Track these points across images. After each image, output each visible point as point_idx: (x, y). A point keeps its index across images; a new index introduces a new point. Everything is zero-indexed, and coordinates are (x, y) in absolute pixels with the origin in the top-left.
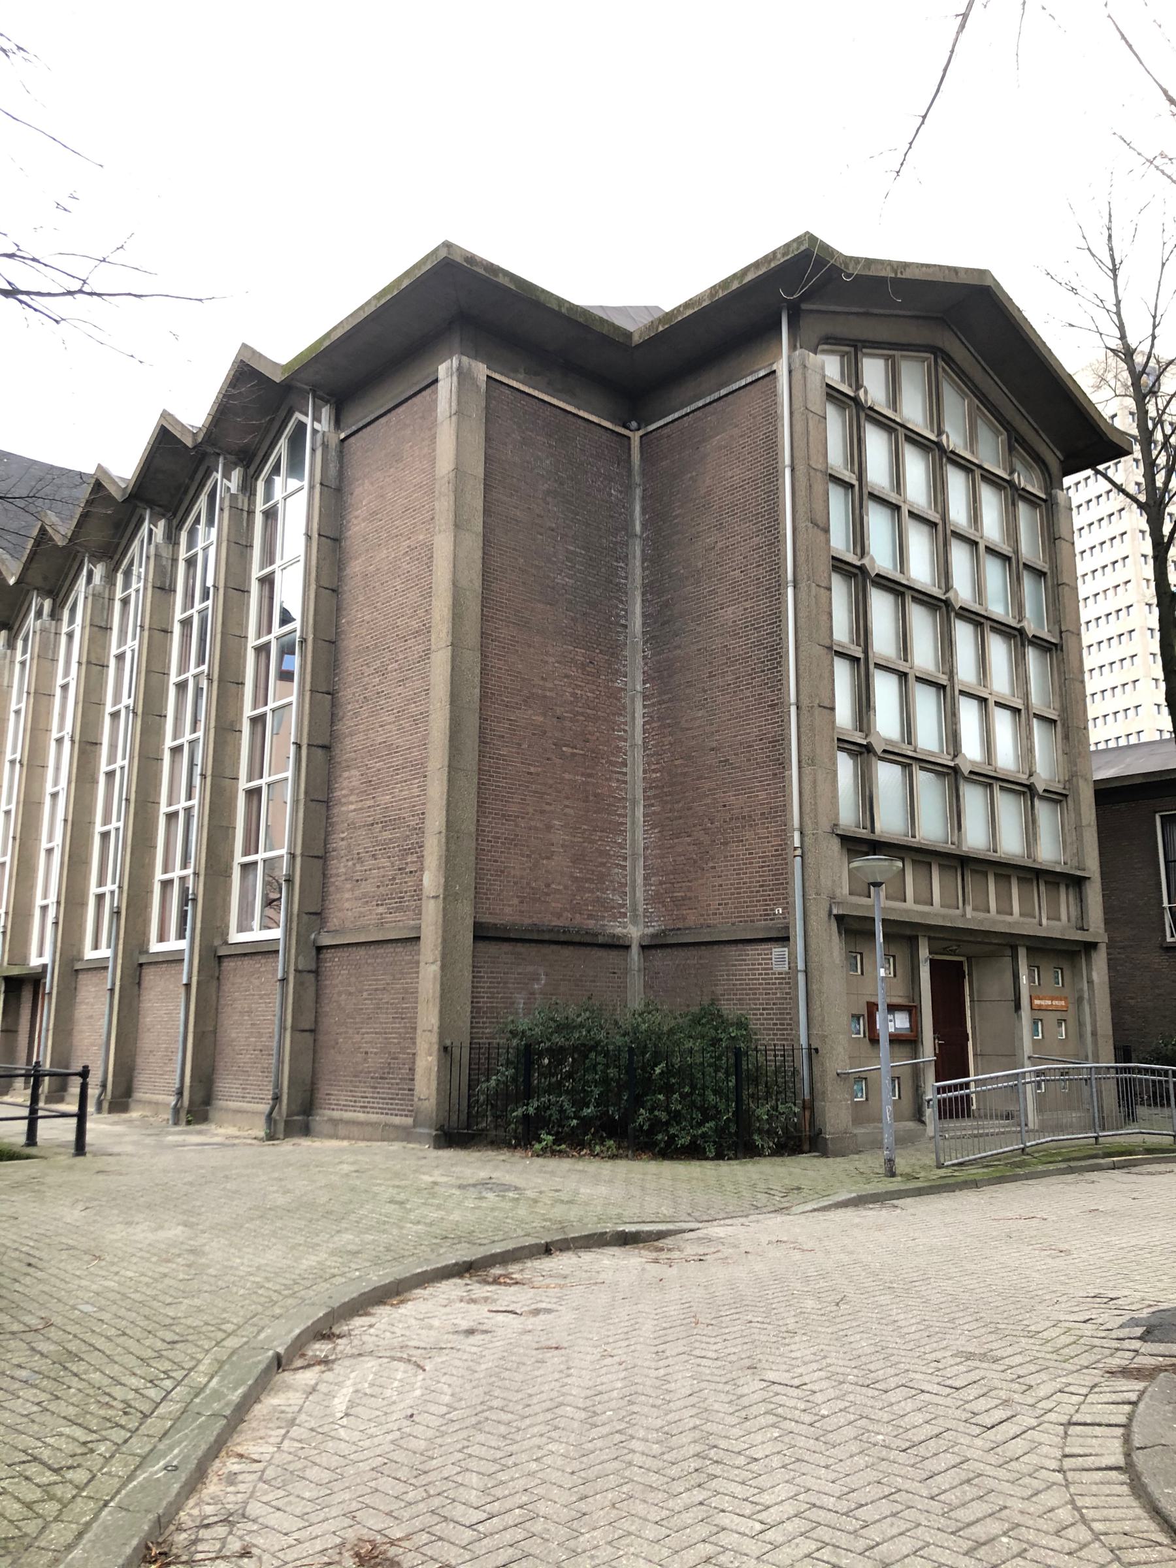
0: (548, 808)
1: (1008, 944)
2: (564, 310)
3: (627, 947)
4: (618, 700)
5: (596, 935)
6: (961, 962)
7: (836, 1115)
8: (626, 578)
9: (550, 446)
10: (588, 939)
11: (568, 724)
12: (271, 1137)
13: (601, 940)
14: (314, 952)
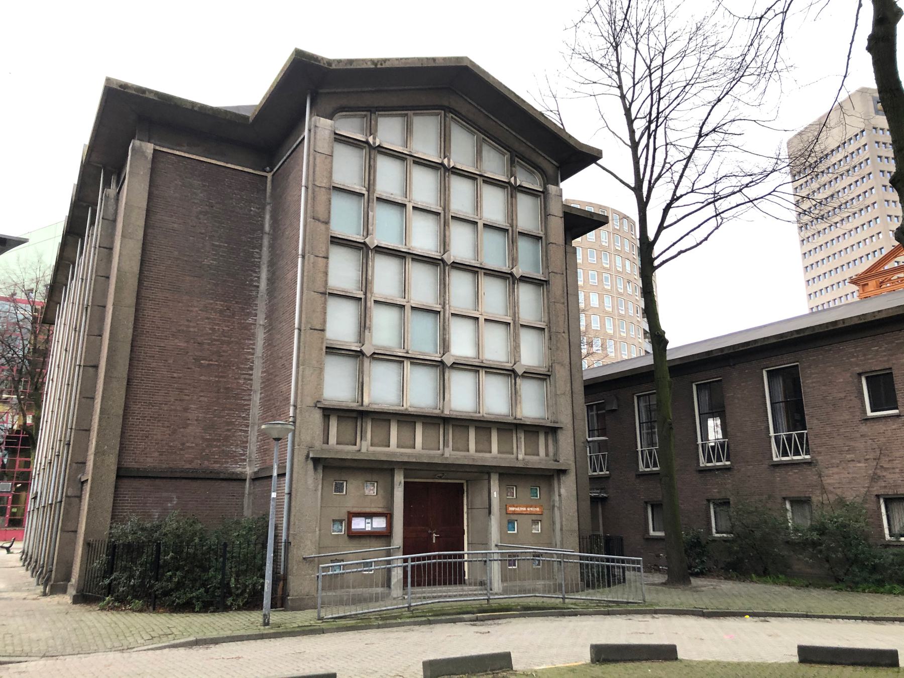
0: (187, 398)
1: (483, 472)
2: (196, 109)
3: (245, 480)
4: (249, 330)
5: (218, 473)
6: (462, 484)
7: (301, 583)
8: (260, 258)
9: (204, 186)
10: (212, 476)
11: (206, 346)
12: (44, 594)
13: (222, 476)
14: (80, 485)
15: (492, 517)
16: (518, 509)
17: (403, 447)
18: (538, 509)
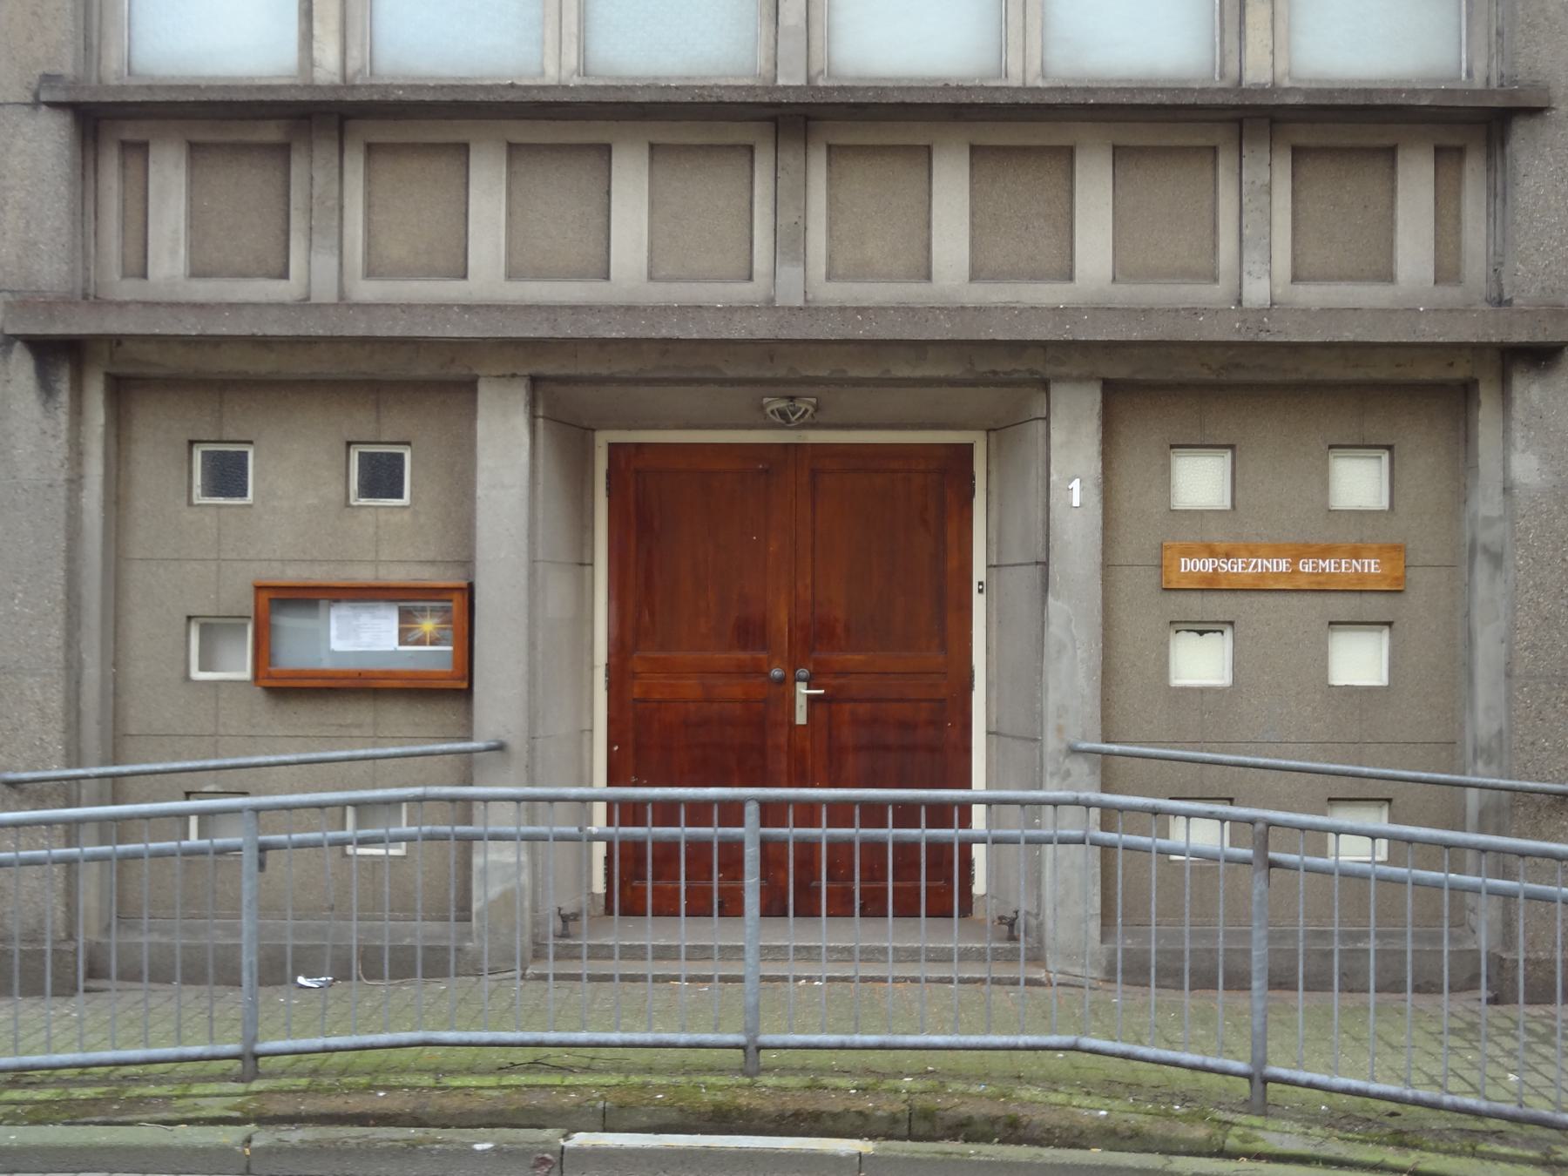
1: (1010, 373)
15: (1056, 606)
16: (1236, 567)
17: (539, 275)
18: (1371, 566)
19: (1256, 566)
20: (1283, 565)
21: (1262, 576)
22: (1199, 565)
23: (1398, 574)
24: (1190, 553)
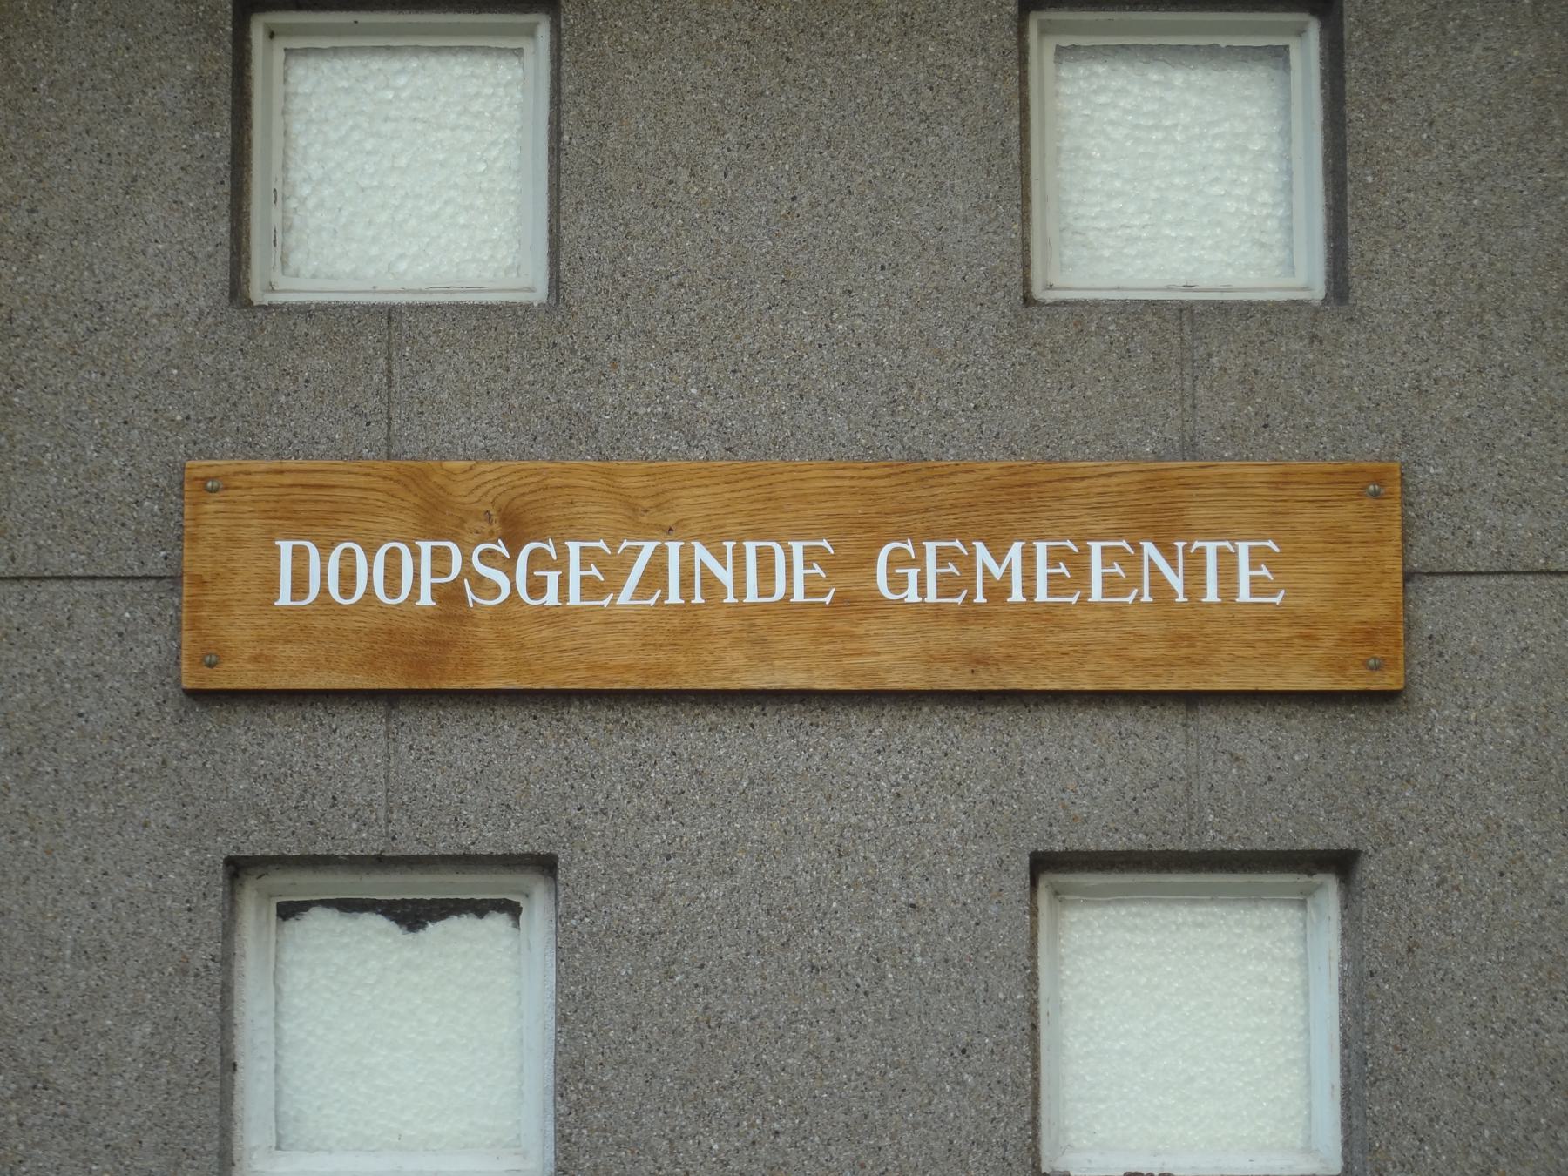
18: (1236, 571)
19: (655, 575)
20: (795, 572)
21: (688, 626)
22: (370, 572)
23: (1376, 608)
24: (319, 516)
